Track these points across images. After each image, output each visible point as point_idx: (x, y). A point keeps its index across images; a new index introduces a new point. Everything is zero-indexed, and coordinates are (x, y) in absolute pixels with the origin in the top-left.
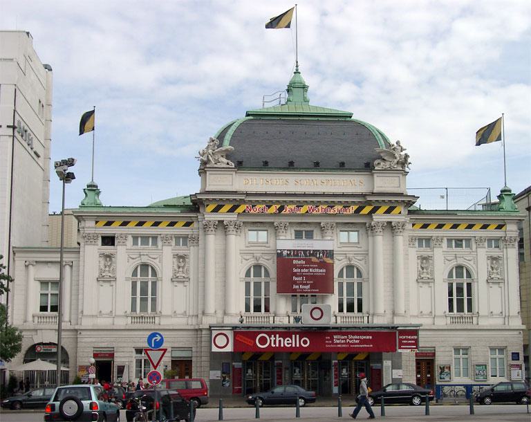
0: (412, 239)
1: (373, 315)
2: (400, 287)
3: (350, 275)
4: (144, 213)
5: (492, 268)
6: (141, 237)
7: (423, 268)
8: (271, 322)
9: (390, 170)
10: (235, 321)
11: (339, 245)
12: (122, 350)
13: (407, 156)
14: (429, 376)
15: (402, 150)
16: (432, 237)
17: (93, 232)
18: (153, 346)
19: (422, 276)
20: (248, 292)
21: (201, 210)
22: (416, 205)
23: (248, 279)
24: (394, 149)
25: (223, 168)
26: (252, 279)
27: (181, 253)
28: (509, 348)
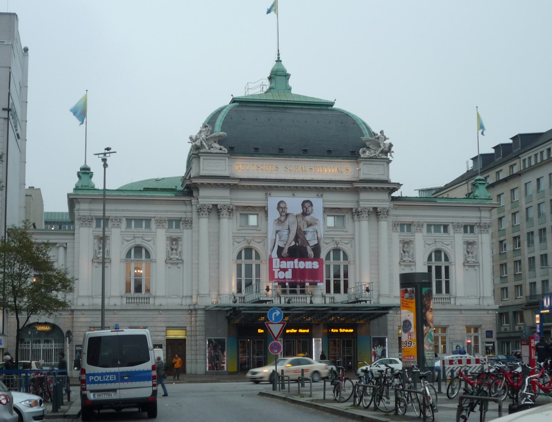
2: (374, 270)
3: (337, 258)
6: (135, 219)
8: (308, 301)
10: (227, 301)
11: (327, 229)
13: (391, 145)
15: (385, 139)
16: (413, 222)
17: (185, 216)
18: (273, 319)
19: (404, 259)
20: (239, 274)
21: (195, 194)
23: (239, 262)
24: (378, 138)
25: (217, 153)
27: (174, 235)
28: (483, 327)
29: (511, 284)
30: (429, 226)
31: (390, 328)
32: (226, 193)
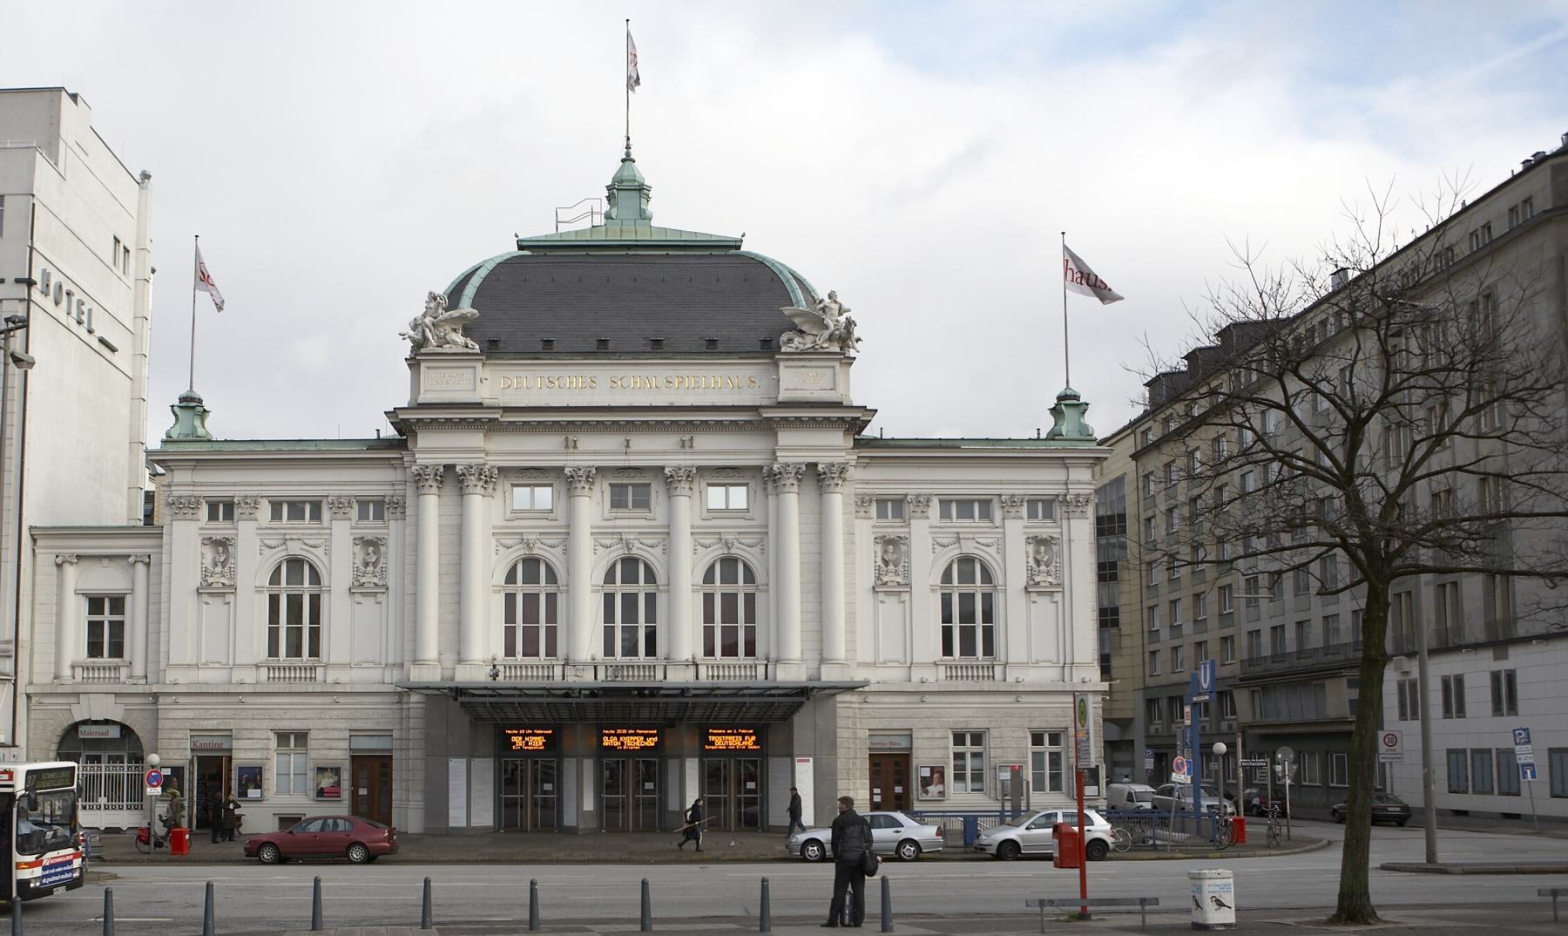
0: (863, 501)
1: (777, 661)
4: (291, 452)
5: (1038, 562)
7: (886, 563)
8: (660, 676)
9: (814, 353)
10: (473, 673)
11: (705, 515)
12: (246, 734)
13: (850, 323)
14: (898, 789)
19: (885, 579)
22: (868, 432)
24: (823, 309)
26: (520, 589)
29: (1213, 635)
30: (945, 503)
31: (842, 733)
32: (475, 440)
